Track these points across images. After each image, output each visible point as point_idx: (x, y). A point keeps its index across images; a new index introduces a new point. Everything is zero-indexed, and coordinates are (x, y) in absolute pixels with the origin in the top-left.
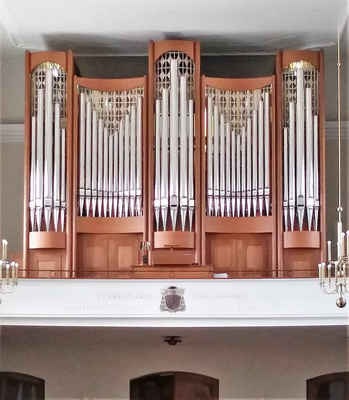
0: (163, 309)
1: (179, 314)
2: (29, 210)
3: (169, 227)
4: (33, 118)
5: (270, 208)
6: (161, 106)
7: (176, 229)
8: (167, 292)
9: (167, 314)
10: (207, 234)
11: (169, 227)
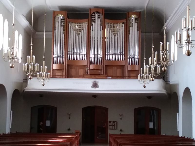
0: (92, 87)
1: (97, 89)
2: (53, 58)
3: (94, 63)
4: (55, 31)
5: (124, 58)
6: (92, 28)
7: (57, 64)
8: (93, 82)
9: (93, 89)
10: (105, 65)
11: (94, 63)
